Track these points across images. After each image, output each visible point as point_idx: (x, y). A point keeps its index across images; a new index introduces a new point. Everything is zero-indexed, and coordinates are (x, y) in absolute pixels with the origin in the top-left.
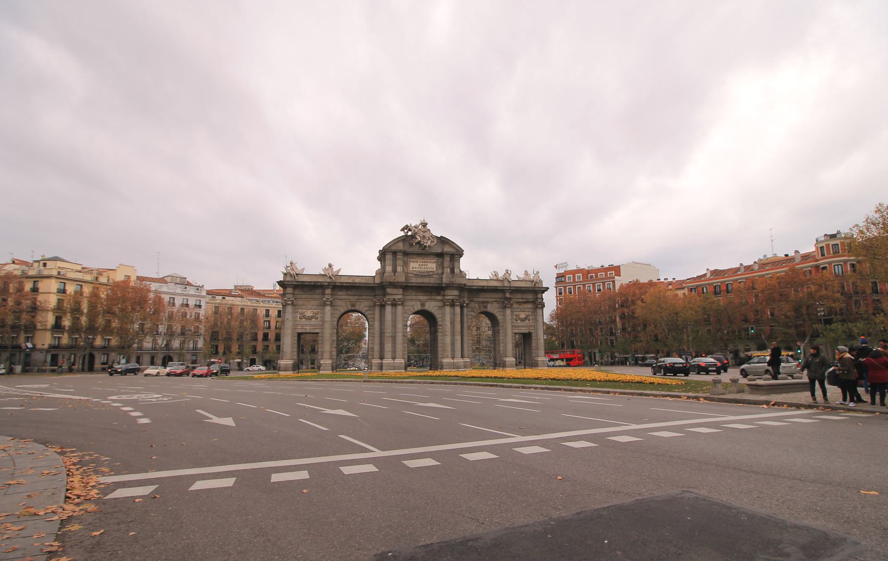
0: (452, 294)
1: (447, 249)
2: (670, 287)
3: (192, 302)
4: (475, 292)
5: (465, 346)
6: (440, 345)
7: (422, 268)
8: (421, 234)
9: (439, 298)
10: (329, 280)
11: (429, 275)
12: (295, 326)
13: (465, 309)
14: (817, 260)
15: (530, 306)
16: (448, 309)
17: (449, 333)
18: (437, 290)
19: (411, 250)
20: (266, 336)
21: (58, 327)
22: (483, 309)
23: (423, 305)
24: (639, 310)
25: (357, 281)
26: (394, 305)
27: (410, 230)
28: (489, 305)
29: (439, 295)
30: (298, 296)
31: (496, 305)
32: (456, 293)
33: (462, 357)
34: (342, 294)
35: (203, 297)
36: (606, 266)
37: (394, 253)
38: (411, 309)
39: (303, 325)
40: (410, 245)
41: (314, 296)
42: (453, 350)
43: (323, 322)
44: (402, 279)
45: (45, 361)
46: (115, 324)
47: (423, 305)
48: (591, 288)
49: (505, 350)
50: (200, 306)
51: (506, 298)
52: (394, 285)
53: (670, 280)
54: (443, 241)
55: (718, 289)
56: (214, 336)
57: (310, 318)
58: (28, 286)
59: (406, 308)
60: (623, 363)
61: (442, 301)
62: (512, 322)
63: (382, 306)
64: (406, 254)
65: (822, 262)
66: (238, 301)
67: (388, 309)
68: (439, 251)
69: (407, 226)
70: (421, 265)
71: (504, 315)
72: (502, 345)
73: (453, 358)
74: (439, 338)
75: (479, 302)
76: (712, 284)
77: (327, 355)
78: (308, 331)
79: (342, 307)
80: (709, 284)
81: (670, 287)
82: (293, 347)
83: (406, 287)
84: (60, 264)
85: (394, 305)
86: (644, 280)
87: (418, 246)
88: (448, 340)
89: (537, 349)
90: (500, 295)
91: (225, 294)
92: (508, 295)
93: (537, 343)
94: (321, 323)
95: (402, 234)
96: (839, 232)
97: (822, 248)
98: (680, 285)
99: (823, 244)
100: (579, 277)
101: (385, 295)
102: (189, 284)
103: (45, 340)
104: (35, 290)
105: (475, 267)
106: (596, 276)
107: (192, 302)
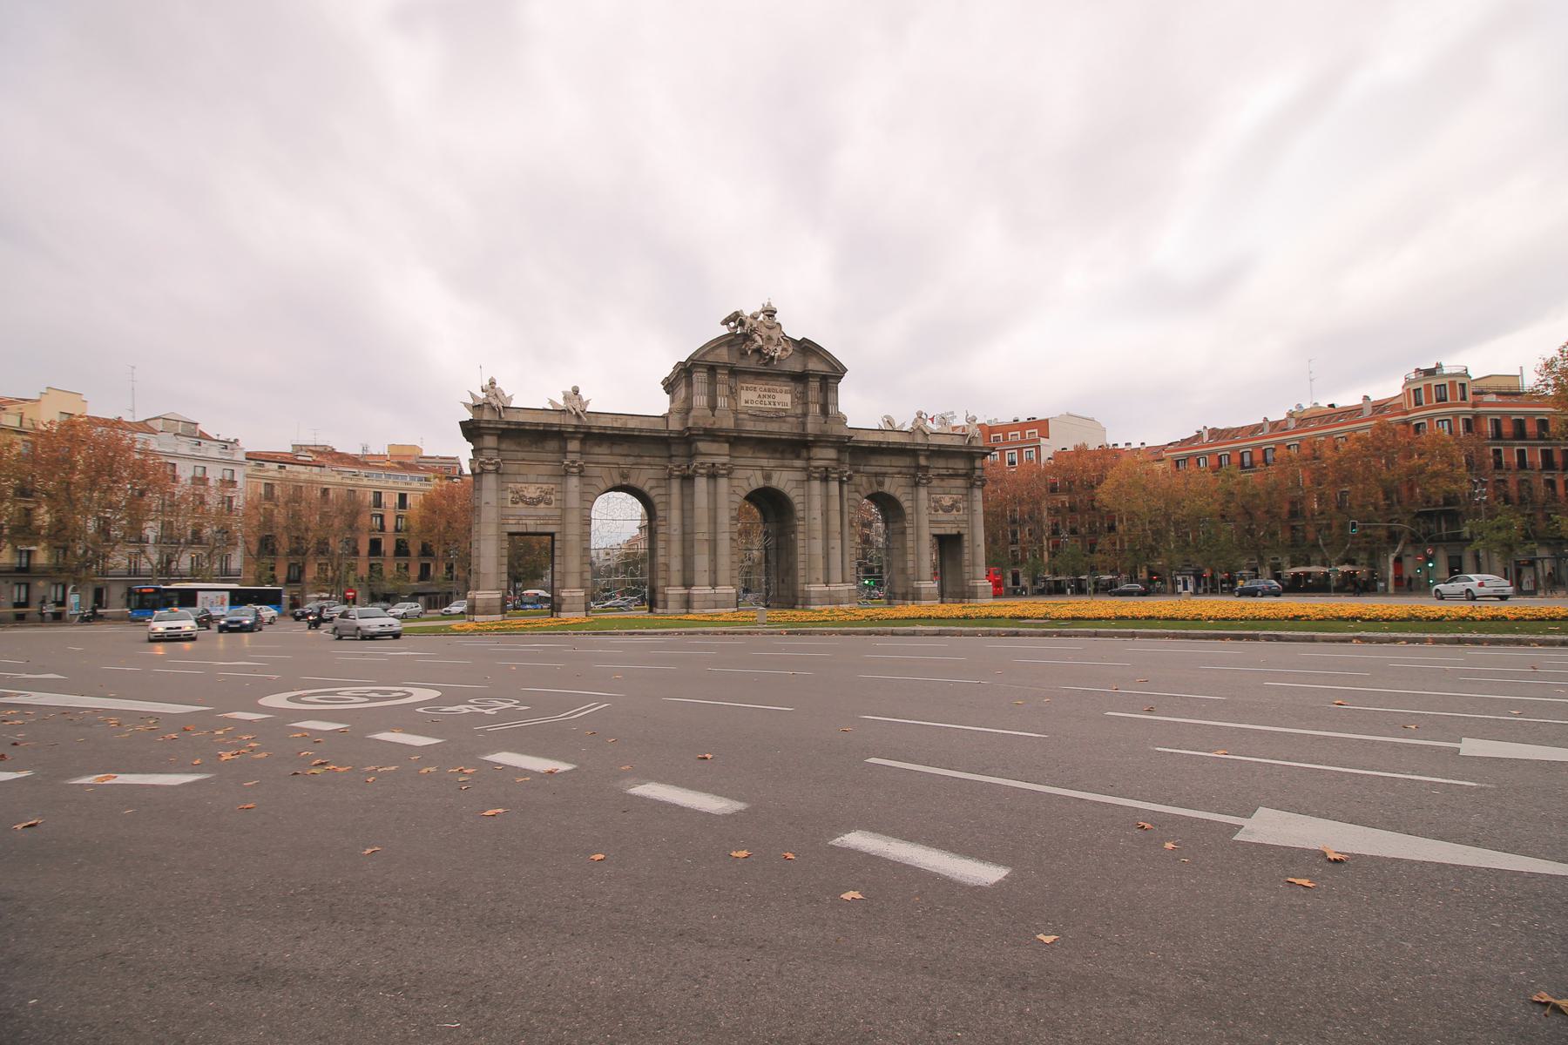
0: (824, 456)
1: (814, 365)
3: (215, 474)
4: (861, 451)
6: (800, 558)
8: (764, 332)
9: (798, 463)
10: (575, 422)
11: (778, 416)
12: (503, 519)
13: (845, 487)
14: (1407, 413)
15: (960, 482)
16: (816, 486)
17: (819, 534)
18: (796, 446)
19: (743, 364)
20: (375, 546)
22: (875, 488)
23: (768, 477)
25: (631, 424)
26: (713, 476)
28: (887, 481)
29: (798, 457)
30: (508, 455)
31: (899, 480)
32: (831, 453)
34: (601, 453)
36: (1023, 419)
37: (712, 369)
38: (745, 484)
39: (520, 517)
41: (543, 456)
42: (827, 569)
43: (564, 510)
44: (728, 423)
46: (44, 517)
47: (768, 477)
48: (1033, 455)
49: (918, 568)
50: (233, 483)
51: (918, 467)
52: (712, 435)
53: (1136, 445)
54: (807, 348)
55: (1247, 459)
56: (267, 545)
59: (735, 482)
60: (1057, 590)
61: (805, 469)
62: (931, 510)
63: (688, 479)
64: (734, 372)
65: (1416, 416)
66: (303, 473)
67: (701, 484)
68: (798, 368)
71: (915, 500)
72: (910, 557)
73: (827, 583)
74: (800, 543)
75: (869, 475)
76: (1215, 453)
77: (573, 580)
78: (531, 530)
80: (1209, 454)
81: (1139, 458)
82: (500, 564)
83: (737, 440)
85: (713, 476)
87: (756, 357)
88: (817, 547)
89: (974, 564)
90: (907, 461)
91: (282, 460)
92: (923, 461)
93: (974, 554)
94: (558, 512)
95: (725, 330)
96: (1439, 366)
97: (1417, 391)
98: (1157, 453)
99: (1421, 385)
101: (692, 455)
102: (204, 436)
105: (860, 408)
107: (215, 474)
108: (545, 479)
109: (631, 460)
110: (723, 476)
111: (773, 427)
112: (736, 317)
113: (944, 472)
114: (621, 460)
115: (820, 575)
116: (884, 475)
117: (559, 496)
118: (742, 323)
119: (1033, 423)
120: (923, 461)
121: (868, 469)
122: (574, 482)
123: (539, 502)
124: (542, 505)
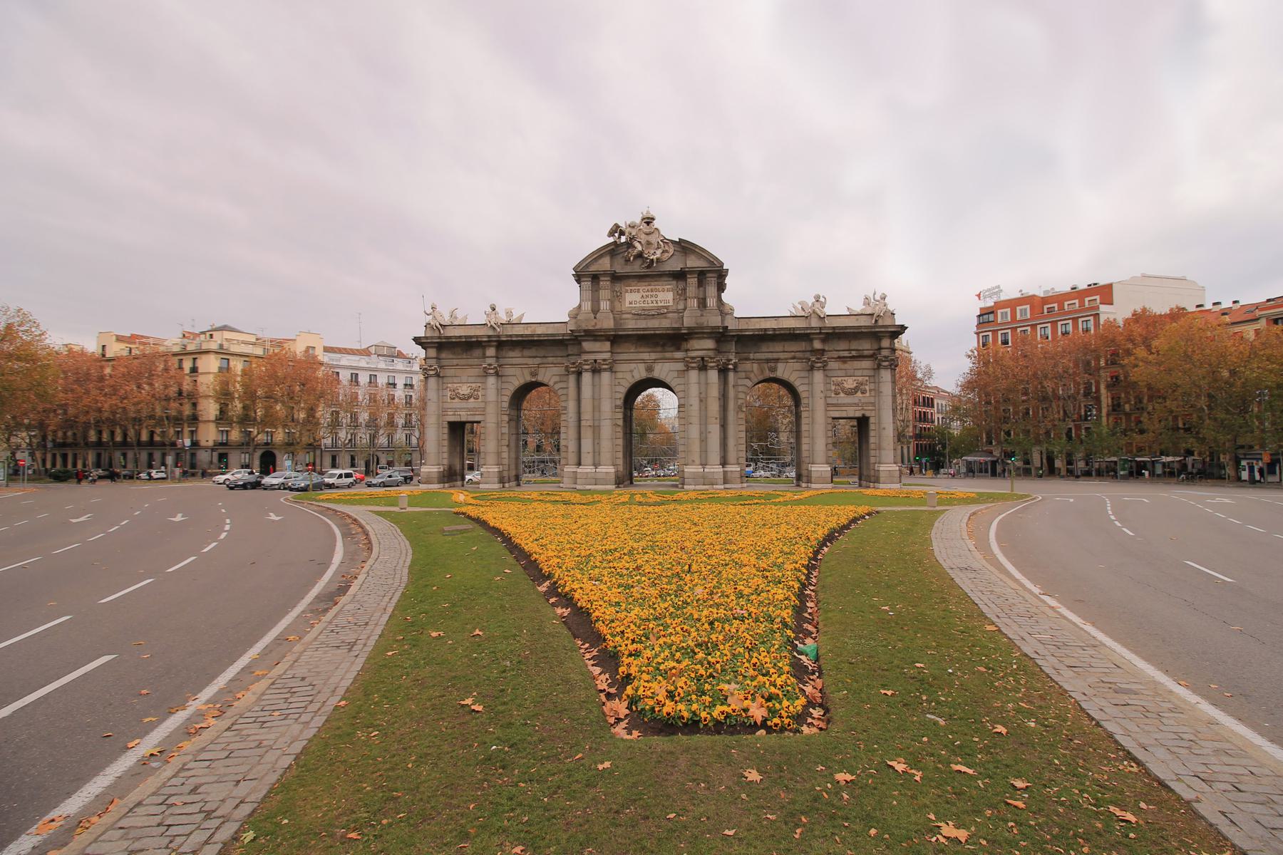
1: (693, 262)
2: (1227, 319)
5: (731, 443)
7: (646, 302)
8: (643, 238)
9: (679, 355)
10: (491, 333)
11: (660, 313)
12: (444, 411)
13: (731, 375)
15: (866, 364)
16: (694, 374)
18: (674, 339)
19: (628, 269)
21: (223, 418)
22: (768, 374)
23: (650, 369)
24: (1141, 370)
25: (540, 330)
26: (596, 371)
27: (622, 233)
28: (780, 366)
29: (678, 349)
32: (710, 344)
33: (724, 463)
34: (514, 356)
35: (416, 373)
36: (1082, 286)
39: (455, 410)
40: (621, 262)
41: (471, 361)
42: (704, 451)
44: (607, 323)
45: (211, 462)
47: (650, 369)
48: (1049, 332)
49: (812, 451)
51: (814, 351)
52: (592, 335)
53: (1226, 304)
54: (685, 247)
57: (466, 398)
58: (187, 365)
59: (620, 375)
62: (826, 396)
63: (579, 374)
64: (616, 278)
67: (587, 377)
69: (617, 226)
70: (653, 299)
71: (811, 384)
79: (517, 378)
83: (617, 339)
84: (227, 335)
85: (596, 371)
86: (1160, 307)
89: (879, 448)
90: (803, 346)
92: (817, 345)
95: (611, 240)
98: (1250, 314)
100: (1024, 312)
103: (209, 435)
104: (194, 370)
105: (752, 296)
106: (1061, 307)
108: (471, 379)
109: (538, 361)
110: (605, 370)
111: (654, 323)
112: (616, 230)
113: (846, 354)
114: (530, 361)
115: (696, 457)
116: (777, 360)
117: (872, 386)
118: (622, 233)
119: (1094, 289)
120: (817, 345)
121: (758, 356)
122: (492, 380)
123: (469, 397)
124: (472, 400)
